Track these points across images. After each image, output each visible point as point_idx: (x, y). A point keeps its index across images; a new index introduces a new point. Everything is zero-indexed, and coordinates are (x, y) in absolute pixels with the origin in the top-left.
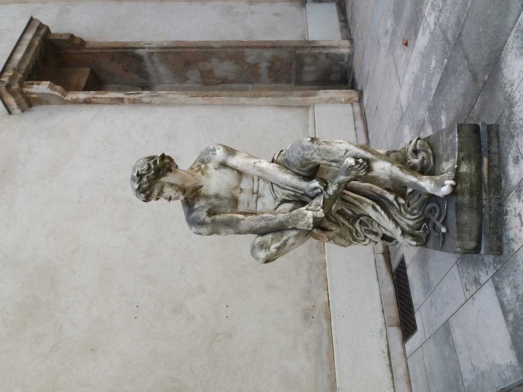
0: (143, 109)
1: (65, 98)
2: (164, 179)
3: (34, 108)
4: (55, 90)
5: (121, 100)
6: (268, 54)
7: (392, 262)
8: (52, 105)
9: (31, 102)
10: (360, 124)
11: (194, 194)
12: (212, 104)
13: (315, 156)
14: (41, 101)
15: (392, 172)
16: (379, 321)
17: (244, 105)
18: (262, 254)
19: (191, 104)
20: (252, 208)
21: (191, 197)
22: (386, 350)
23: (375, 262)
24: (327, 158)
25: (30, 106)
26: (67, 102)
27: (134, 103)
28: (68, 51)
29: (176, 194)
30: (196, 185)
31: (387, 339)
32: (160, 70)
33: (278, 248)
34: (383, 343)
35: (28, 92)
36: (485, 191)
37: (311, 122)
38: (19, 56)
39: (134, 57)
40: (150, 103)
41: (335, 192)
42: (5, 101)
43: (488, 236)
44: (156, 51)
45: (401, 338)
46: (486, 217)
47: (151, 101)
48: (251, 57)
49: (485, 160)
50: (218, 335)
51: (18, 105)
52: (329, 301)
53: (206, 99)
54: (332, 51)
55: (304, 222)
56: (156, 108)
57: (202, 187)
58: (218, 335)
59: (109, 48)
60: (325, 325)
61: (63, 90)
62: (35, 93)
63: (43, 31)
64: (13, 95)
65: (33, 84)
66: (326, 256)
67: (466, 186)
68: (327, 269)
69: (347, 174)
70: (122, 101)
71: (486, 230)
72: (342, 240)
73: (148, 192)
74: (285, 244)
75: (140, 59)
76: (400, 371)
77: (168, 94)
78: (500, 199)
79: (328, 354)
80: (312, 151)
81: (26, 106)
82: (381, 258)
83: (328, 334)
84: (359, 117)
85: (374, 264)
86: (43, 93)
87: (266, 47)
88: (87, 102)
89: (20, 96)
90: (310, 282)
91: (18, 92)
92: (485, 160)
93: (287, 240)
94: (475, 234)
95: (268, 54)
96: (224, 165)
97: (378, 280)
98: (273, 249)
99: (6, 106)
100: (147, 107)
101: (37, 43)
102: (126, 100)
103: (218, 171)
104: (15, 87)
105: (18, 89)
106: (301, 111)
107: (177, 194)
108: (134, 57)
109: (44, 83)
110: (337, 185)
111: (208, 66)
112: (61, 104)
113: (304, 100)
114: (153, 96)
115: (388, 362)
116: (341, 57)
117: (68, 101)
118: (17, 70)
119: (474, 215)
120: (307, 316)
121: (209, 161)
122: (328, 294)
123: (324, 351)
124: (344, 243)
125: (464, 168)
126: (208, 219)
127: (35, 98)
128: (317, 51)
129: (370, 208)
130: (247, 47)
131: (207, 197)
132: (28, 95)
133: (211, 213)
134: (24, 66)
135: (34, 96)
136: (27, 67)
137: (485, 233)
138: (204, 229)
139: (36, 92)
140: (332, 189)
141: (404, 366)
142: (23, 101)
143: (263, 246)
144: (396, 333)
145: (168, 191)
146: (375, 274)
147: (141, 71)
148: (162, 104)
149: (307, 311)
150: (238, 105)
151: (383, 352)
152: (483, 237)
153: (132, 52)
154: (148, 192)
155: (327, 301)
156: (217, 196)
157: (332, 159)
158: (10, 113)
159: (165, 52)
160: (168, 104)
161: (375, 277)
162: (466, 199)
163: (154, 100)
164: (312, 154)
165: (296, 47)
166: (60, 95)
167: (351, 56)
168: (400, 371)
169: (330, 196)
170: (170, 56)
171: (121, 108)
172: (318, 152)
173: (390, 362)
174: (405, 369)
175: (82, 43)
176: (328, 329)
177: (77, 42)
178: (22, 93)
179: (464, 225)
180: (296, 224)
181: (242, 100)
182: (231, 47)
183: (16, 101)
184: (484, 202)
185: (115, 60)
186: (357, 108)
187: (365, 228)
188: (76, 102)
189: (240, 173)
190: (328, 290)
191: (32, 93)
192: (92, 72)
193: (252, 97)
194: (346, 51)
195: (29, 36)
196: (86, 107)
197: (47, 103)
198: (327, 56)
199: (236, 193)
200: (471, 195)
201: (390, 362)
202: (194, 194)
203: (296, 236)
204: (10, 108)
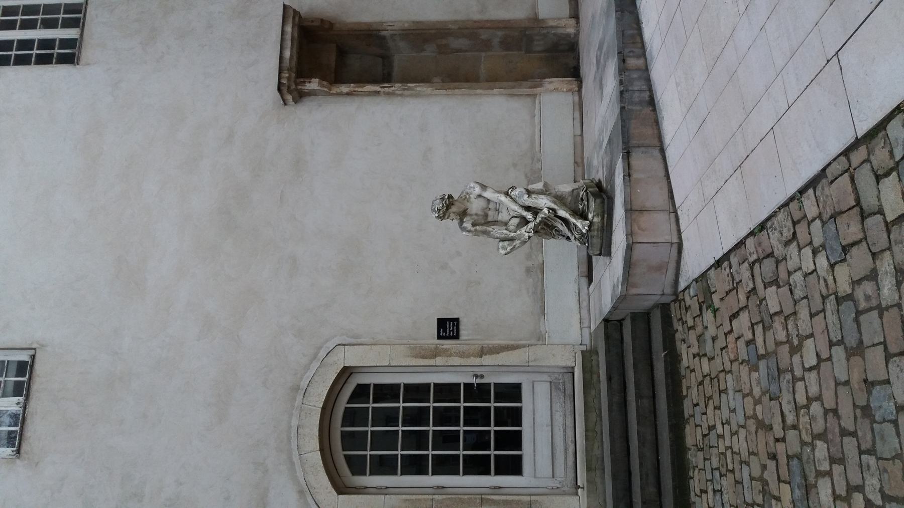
0: (397, 100)
2: (450, 210)
6: (500, 33)
10: (577, 115)
12: (454, 95)
14: (312, 93)
16: (576, 273)
17: (481, 95)
18: (503, 252)
19: (436, 95)
20: (495, 219)
26: (333, 94)
32: (402, 56)
34: (576, 287)
37: (537, 112)
38: (287, 54)
40: (401, 95)
48: (485, 35)
54: (560, 31)
56: (408, 99)
60: (540, 276)
65: (305, 82)
67: (596, 227)
75: (384, 38)
76: (584, 304)
77: (416, 87)
84: (577, 107)
87: (498, 28)
95: (500, 33)
96: (480, 196)
98: (508, 249)
106: (529, 100)
109: (313, 80)
111: (444, 42)
114: (404, 90)
116: (568, 35)
120: (528, 270)
123: (539, 292)
125: (596, 220)
126: (473, 229)
128: (545, 31)
130: (481, 28)
131: (471, 215)
133: (474, 225)
140: (538, 220)
143: (503, 248)
144: (584, 281)
145: (452, 216)
147: (386, 59)
148: (411, 96)
150: (476, 95)
156: (476, 214)
158: (285, 104)
160: (418, 95)
162: (595, 233)
163: (406, 92)
165: (526, 29)
167: (577, 34)
168: (584, 304)
171: (378, 99)
175: (331, 24)
177: (326, 26)
181: (479, 91)
182: (467, 28)
186: (576, 98)
188: (341, 94)
189: (489, 201)
192: (337, 46)
193: (488, 89)
194: (571, 31)
195: (289, 29)
196: (348, 99)
198: (555, 34)
199: (486, 211)
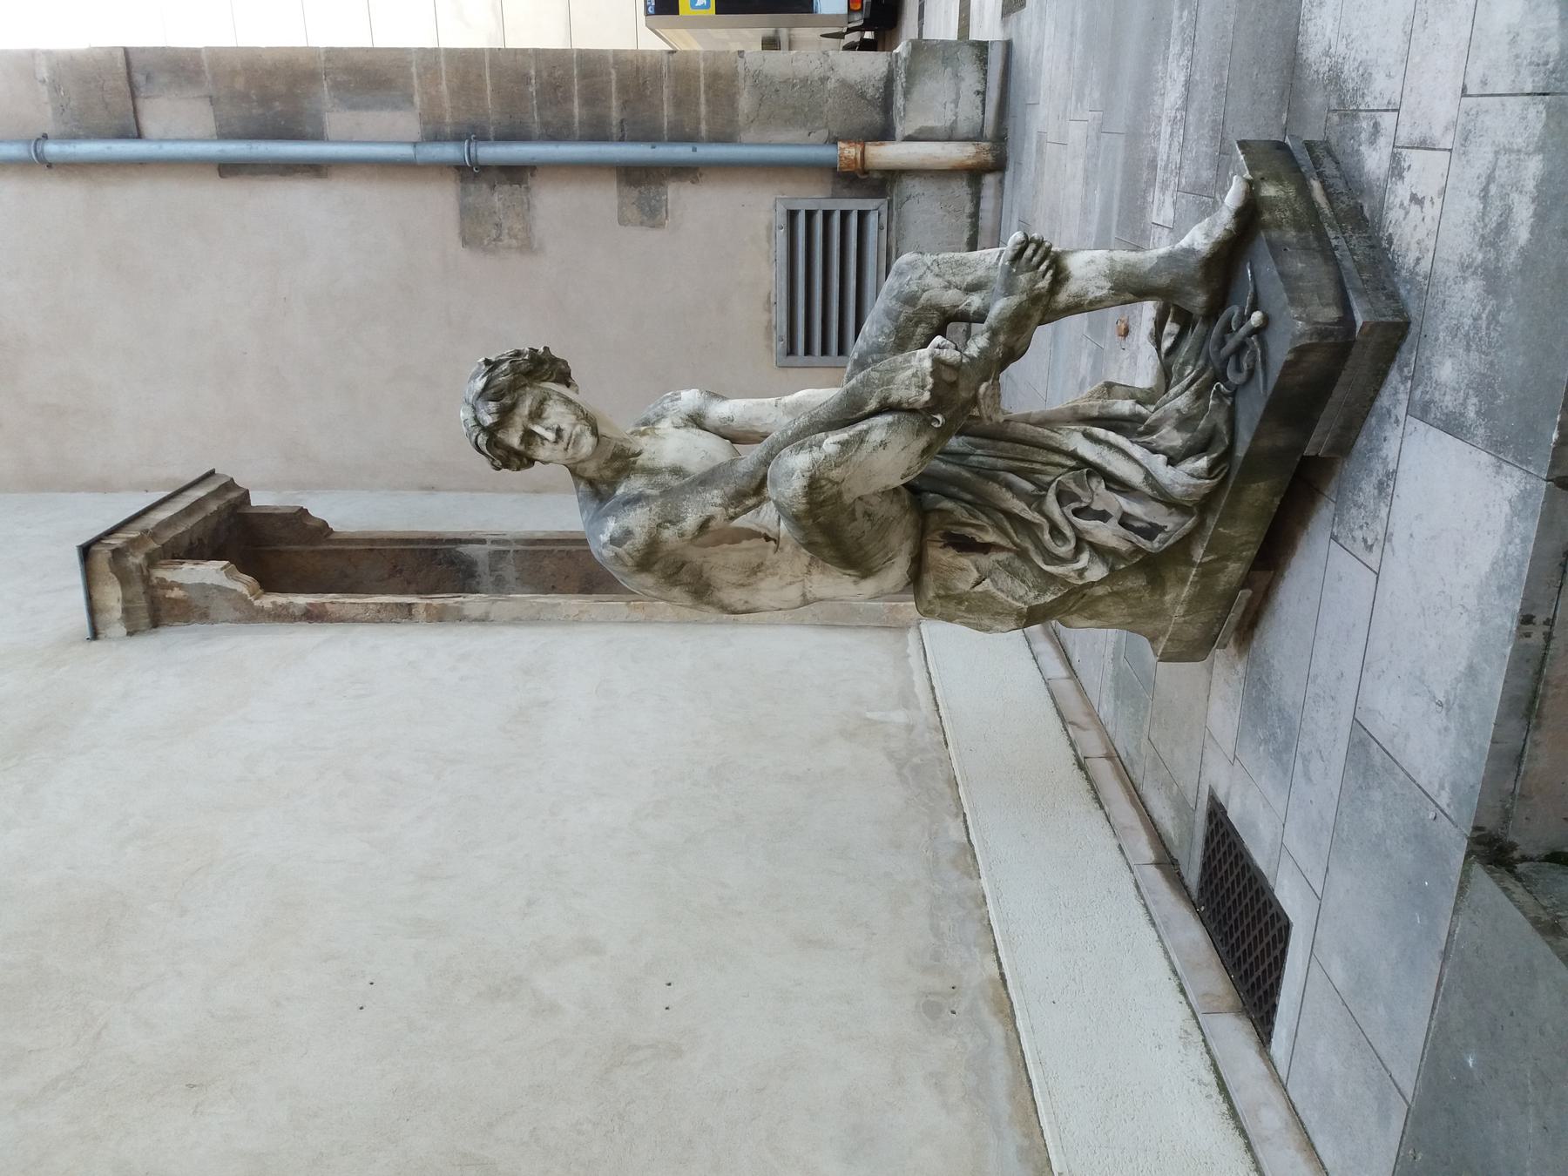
1: (257, 603)
3: (161, 630)
4: (237, 580)
5: (407, 612)
7: (1186, 881)
8: (214, 622)
9: (162, 613)
11: (617, 464)
13: (930, 279)
15: (1112, 260)
21: (608, 473)
22: (1210, 1078)
23: (1137, 887)
24: (957, 280)
25: (156, 623)
27: (441, 620)
28: (283, 547)
29: (574, 425)
30: (627, 445)
31: (1209, 1052)
33: (844, 444)
35: (163, 580)
36: (1332, 227)
39: (452, 563)
40: (483, 620)
41: (982, 351)
42: (96, 596)
43: (1362, 293)
44: (512, 548)
45: (1255, 1038)
46: (1348, 264)
47: (487, 614)
49: (1316, 185)
50: (637, 1048)
51: (125, 610)
52: (1002, 975)
53: (635, 607)
55: (909, 372)
57: (639, 454)
58: (637, 1048)
59: (392, 541)
60: (997, 1031)
61: (256, 584)
62: (181, 586)
63: (233, 495)
64: (124, 579)
66: (984, 881)
68: (990, 907)
69: (1009, 290)
70: (410, 611)
71: (1353, 282)
72: (1017, 582)
73: (507, 401)
74: (861, 438)
76: (1269, 1120)
78: (1369, 238)
79: (1012, 1096)
80: (920, 272)
81: (144, 618)
82: (1154, 876)
83: (1009, 1050)
85: (1134, 892)
86: (202, 586)
88: (312, 616)
89: (139, 588)
90: (936, 931)
91: (136, 575)
92: (1316, 185)
93: (867, 432)
94: (1330, 292)
97: (1154, 924)
99: (92, 610)
100: (475, 628)
101: (213, 506)
102: (420, 612)
103: (682, 431)
104: (136, 559)
105: (140, 567)
107: (578, 428)
108: (452, 563)
110: (987, 335)
112: (238, 621)
113: (891, 609)
115: (1225, 1107)
117: (262, 609)
118: (153, 534)
119: (1318, 260)
120: (933, 1009)
121: (661, 417)
122: (998, 959)
124: (1022, 593)
127: (176, 601)
129: (1079, 436)
132: (160, 592)
134: (169, 534)
135: (176, 593)
136: (175, 537)
137: (1355, 290)
138: (639, 511)
139: (187, 581)
141: (1281, 1105)
142: (142, 603)
144: (1233, 1033)
146: (1141, 911)
149: (931, 998)
151: (1200, 1082)
152: (1354, 305)
153: (449, 550)
154: (507, 401)
155: (998, 977)
156: (677, 471)
157: (969, 279)
158: (95, 635)
159: (535, 552)
161: (1144, 919)
164: (920, 278)
166: (246, 592)
168: (1269, 1120)
169: (972, 358)
170: (546, 562)
172: (936, 269)
173: (1232, 1107)
174: (1285, 1114)
176: (1007, 1037)
178: (146, 580)
179: (1300, 277)
180: (889, 382)
183: (125, 600)
184: (1334, 242)
185: (401, 571)
187: (1074, 505)
190: (996, 950)
191: (171, 586)
197: (204, 616)
200: (1300, 228)
201: (1232, 1107)
202: (617, 464)
203: (890, 425)
204: (101, 619)
